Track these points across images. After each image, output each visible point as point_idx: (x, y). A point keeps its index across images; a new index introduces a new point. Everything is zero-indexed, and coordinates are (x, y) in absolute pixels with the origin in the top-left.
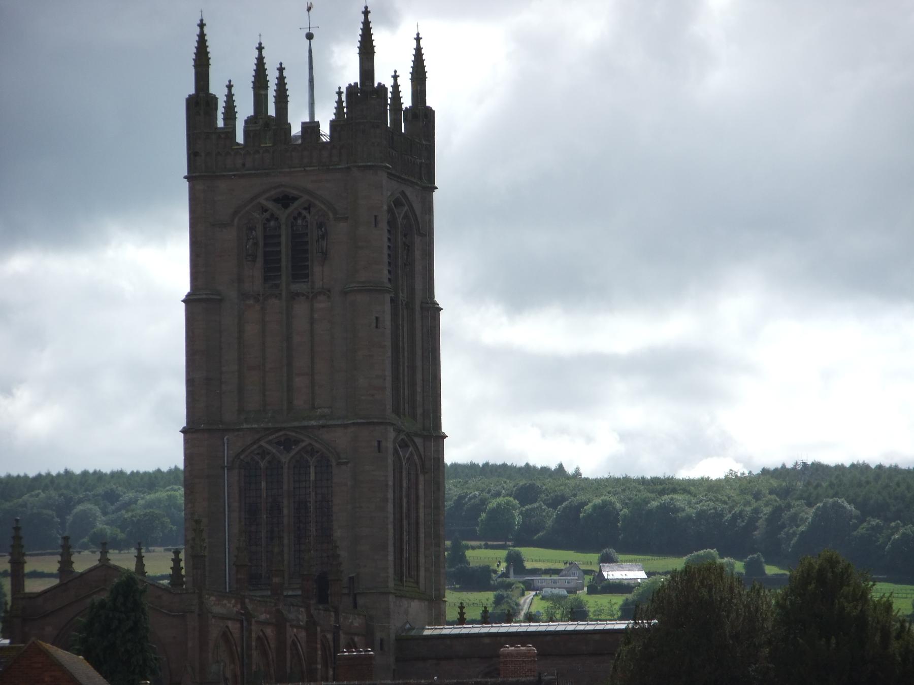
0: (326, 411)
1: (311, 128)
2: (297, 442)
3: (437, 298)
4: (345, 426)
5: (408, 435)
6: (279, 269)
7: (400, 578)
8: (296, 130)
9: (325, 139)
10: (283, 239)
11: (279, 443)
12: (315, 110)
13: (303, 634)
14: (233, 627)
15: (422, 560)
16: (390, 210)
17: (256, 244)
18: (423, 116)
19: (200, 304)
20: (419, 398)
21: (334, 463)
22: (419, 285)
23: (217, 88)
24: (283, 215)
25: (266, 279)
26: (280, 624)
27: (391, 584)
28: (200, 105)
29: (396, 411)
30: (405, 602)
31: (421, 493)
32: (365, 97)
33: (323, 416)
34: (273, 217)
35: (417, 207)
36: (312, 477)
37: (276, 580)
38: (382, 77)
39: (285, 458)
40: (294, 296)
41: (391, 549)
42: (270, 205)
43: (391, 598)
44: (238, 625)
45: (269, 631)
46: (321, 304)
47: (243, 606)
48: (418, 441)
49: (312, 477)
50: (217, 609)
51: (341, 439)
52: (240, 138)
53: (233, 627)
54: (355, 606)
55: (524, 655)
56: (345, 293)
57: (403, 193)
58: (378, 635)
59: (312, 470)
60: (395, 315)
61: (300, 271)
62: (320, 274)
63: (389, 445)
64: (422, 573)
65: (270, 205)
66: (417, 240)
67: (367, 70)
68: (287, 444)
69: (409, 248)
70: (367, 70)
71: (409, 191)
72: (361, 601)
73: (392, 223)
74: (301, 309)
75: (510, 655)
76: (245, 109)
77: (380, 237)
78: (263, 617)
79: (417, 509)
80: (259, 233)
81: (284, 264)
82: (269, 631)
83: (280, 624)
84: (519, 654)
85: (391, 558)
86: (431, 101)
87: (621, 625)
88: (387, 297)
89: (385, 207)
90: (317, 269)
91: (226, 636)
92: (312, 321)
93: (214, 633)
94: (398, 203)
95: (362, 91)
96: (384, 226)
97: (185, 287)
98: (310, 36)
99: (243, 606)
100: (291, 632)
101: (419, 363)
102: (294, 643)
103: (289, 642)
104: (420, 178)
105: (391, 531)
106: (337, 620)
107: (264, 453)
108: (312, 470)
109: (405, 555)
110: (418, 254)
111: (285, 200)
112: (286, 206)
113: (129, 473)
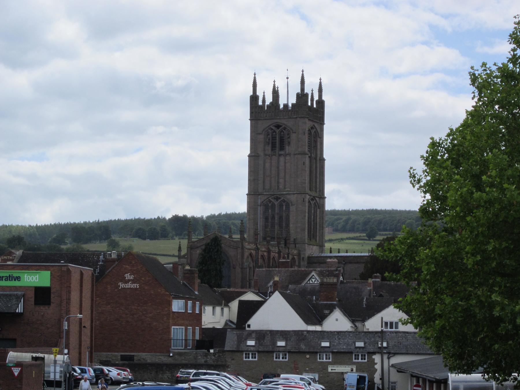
0: (289, 189)
1: (286, 106)
2: (280, 198)
3: (324, 157)
4: (294, 194)
5: (314, 197)
6: (276, 147)
7: (310, 238)
8: (281, 106)
9: (290, 109)
10: (277, 138)
11: (275, 199)
12: (288, 99)
13: (277, 255)
14: (253, 252)
15: (318, 234)
16: (309, 130)
17: (269, 140)
18: (321, 103)
19: (253, 157)
20: (318, 186)
21: (290, 204)
22: (319, 152)
23: (260, 93)
24: (277, 131)
25: (272, 150)
26: (269, 252)
27: (306, 241)
28: (254, 98)
29: (310, 190)
30: (311, 246)
31: (318, 214)
32: (302, 96)
33: (288, 191)
34: (274, 132)
35: (319, 130)
36: (284, 209)
37: (268, 239)
38: (307, 90)
39: (276, 203)
40: (280, 155)
41: (306, 231)
42: (274, 128)
43: (306, 245)
44: (255, 252)
45: (265, 254)
46: (288, 158)
47: (257, 246)
48: (317, 199)
49: (284, 209)
50: (248, 247)
51: (293, 198)
52: (315, 106)
53: (253, 252)
54: (295, 247)
55: (334, 262)
56: (295, 154)
57: (314, 125)
58: (302, 256)
59: (284, 207)
60: (310, 161)
61: (282, 148)
62: (287, 149)
63: (307, 200)
64: (318, 237)
65: (274, 128)
66: (319, 139)
67: (303, 89)
68: (277, 199)
69: (316, 142)
70: (303, 89)
71: (316, 125)
72: (297, 246)
73: (310, 134)
74: (282, 159)
75: (329, 262)
76: (269, 100)
77: (306, 138)
78: (263, 249)
79: (317, 219)
80: (270, 136)
81: (277, 146)
82: (265, 254)
83: (269, 252)
84: (332, 262)
85: (306, 233)
86: (324, 98)
87: (367, 254)
88: (307, 156)
89: (307, 129)
90: (287, 147)
91: (251, 254)
92: (285, 163)
93: (246, 254)
94: (312, 128)
95: (301, 94)
96: (307, 135)
97: (248, 152)
98: (287, 78)
99: (257, 246)
100: (272, 254)
101: (318, 176)
102: (274, 257)
103: (272, 257)
104: (320, 121)
105: (307, 226)
106: (288, 251)
107: (270, 201)
108: (284, 207)
109: (312, 233)
110: (318, 144)
111: (278, 126)
112: (278, 128)
113: (411, 199)
